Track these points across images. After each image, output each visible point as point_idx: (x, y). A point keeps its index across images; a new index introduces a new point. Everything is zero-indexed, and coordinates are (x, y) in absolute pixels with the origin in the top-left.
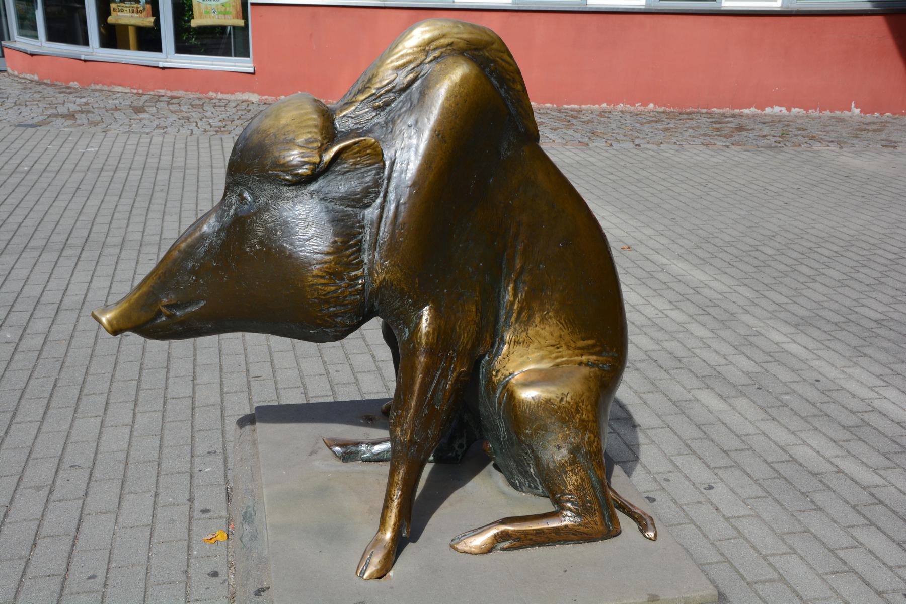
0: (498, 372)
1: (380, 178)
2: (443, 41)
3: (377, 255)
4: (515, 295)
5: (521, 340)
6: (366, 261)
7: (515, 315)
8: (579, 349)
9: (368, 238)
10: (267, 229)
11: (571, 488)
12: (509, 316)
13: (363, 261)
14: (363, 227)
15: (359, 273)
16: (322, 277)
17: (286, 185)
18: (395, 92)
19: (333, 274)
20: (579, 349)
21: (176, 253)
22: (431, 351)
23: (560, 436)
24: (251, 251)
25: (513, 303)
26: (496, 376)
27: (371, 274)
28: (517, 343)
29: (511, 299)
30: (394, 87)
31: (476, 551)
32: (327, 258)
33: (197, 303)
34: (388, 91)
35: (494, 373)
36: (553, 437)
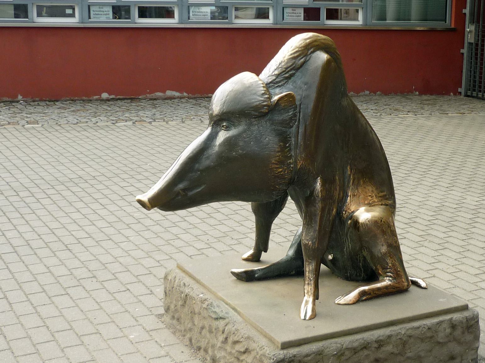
0: (346, 211)
1: (296, 112)
2: (316, 43)
3: (298, 151)
4: (351, 172)
5: (356, 194)
6: (293, 155)
7: (351, 181)
8: (380, 197)
9: (293, 143)
10: (245, 142)
11: (390, 265)
12: (349, 182)
13: (292, 155)
14: (290, 137)
15: (291, 161)
16: (277, 164)
17: (254, 118)
18: (294, 70)
19: (281, 162)
20: (380, 197)
21: (360, 115)
22: (324, 199)
23: (383, 239)
24: (236, 154)
25: (350, 175)
26: (345, 213)
27: (296, 162)
28: (354, 195)
29: (350, 173)
30: (294, 67)
31: (351, 302)
32: (278, 154)
33: (200, 186)
34: (291, 70)
35: (344, 212)
36: (379, 241)
